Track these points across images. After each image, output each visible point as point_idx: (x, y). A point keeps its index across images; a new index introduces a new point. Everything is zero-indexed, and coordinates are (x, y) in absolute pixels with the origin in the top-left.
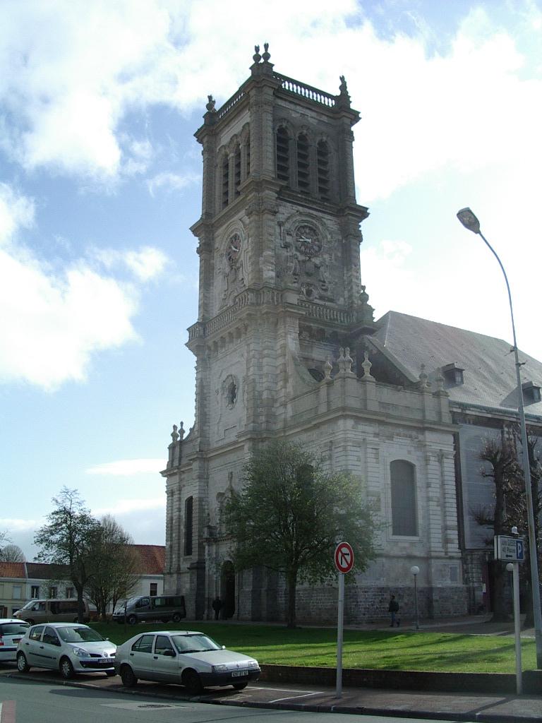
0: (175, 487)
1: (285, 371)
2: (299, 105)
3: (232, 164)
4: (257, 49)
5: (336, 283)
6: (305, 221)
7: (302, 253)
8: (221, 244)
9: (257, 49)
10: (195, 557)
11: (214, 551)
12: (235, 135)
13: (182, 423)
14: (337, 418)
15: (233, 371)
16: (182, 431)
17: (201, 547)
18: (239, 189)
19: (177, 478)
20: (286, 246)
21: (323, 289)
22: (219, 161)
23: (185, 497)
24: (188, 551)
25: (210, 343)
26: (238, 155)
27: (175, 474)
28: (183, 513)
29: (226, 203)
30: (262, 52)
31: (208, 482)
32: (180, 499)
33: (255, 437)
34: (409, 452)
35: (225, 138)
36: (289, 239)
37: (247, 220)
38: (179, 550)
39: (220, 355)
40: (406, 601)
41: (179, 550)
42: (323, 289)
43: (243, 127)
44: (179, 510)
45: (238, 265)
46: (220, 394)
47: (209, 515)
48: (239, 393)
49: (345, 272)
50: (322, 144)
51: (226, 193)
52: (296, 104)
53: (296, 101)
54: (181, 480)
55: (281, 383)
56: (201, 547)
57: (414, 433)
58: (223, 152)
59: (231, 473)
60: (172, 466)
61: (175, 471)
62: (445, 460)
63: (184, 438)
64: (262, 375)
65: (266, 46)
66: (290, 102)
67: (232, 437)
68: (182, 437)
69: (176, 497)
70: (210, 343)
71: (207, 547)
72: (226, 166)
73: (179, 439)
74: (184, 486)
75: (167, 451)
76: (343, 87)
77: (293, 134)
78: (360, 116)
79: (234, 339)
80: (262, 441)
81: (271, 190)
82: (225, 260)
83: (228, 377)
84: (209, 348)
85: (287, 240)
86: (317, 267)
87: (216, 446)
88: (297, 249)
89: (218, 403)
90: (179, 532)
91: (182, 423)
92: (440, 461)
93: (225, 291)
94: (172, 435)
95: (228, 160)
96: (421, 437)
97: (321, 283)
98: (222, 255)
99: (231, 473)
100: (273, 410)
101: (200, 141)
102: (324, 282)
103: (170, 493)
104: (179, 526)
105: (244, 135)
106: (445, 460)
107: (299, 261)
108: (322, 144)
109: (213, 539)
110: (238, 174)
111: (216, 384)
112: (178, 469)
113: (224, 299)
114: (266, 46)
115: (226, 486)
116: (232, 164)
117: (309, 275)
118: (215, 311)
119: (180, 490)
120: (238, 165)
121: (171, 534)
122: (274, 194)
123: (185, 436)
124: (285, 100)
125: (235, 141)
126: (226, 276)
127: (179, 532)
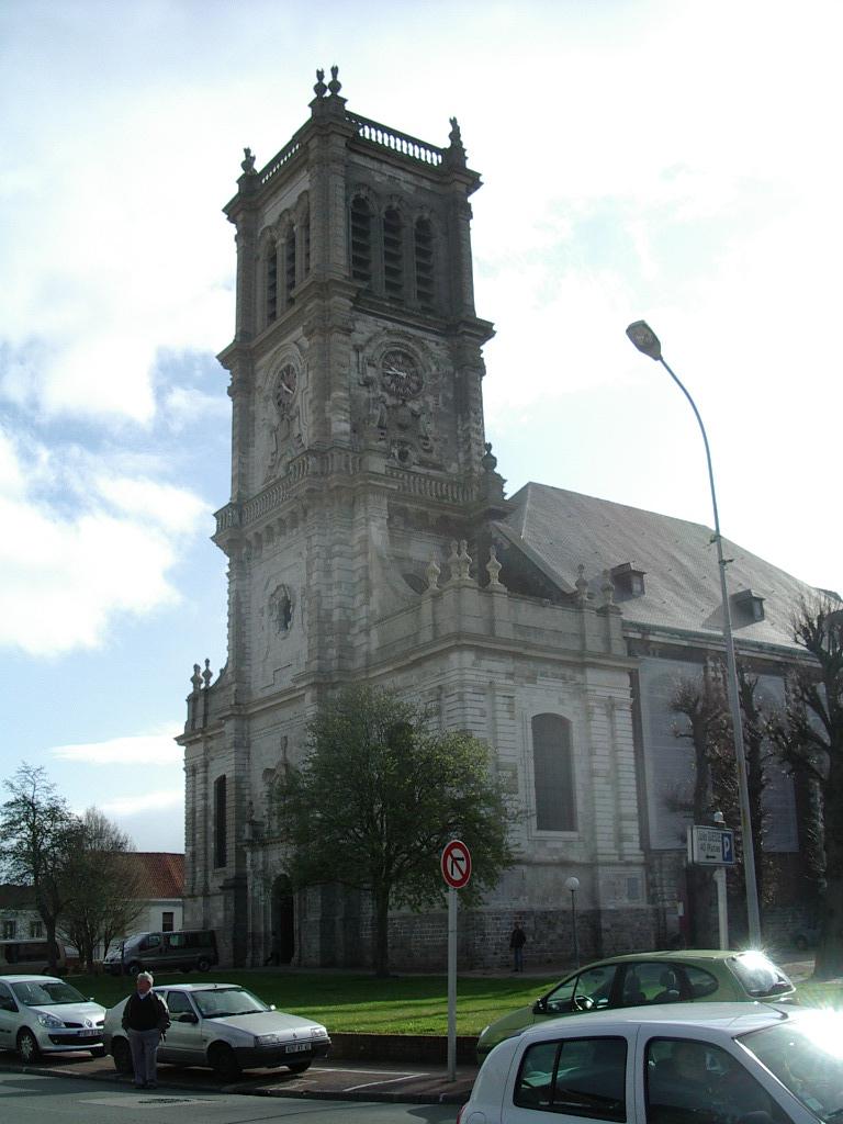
0: (199, 761)
1: (367, 578)
2: (386, 163)
3: (282, 254)
4: (320, 75)
5: (445, 441)
6: (398, 344)
7: (391, 393)
8: (265, 380)
9: (320, 75)
10: (230, 870)
11: (261, 860)
12: (286, 210)
13: (207, 662)
14: (450, 650)
15: (286, 579)
16: (208, 674)
17: (240, 855)
18: (293, 294)
19: (200, 748)
20: (368, 383)
21: (425, 450)
22: (262, 251)
23: (214, 776)
24: (221, 860)
25: (250, 536)
26: (292, 242)
27: (197, 741)
28: (211, 802)
29: (273, 316)
30: (327, 80)
31: (249, 753)
32: (206, 781)
33: (322, 680)
34: (561, 701)
35: (271, 216)
36: (371, 372)
37: (306, 343)
38: (206, 859)
39: (265, 555)
40: (560, 931)
41: (206, 859)
42: (425, 450)
43: (300, 197)
44: (205, 797)
45: (292, 413)
46: (266, 615)
47: (251, 803)
48: (296, 613)
49: (459, 422)
50: (422, 225)
51: (273, 302)
52: (381, 161)
53: (381, 157)
54: (207, 751)
55: (360, 597)
56: (240, 855)
57: (569, 672)
58: (268, 236)
59: (286, 737)
60: (193, 729)
61: (199, 736)
62: (617, 713)
63: (211, 685)
64: (331, 585)
65: (335, 71)
66: (373, 158)
67: (286, 682)
68: (207, 682)
69: (200, 776)
70: (250, 536)
71: (249, 854)
72: (273, 259)
73: (203, 686)
74: (212, 759)
75: (185, 706)
76: (455, 135)
77: (378, 209)
78: (481, 179)
79: (288, 530)
80: (333, 688)
81: (343, 296)
82: (272, 406)
83: (278, 588)
84: (249, 543)
85: (369, 374)
86: (415, 416)
87: (260, 695)
88: (384, 388)
89: (263, 625)
90: (206, 832)
91: (207, 662)
92: (610, 715)
93: (273, 454)
94: (192, 680)
95: (275, 250)
96: (579, 677)
97: (422, 441)
98: (266, 399)
99: (286, 737)
100: (349, 638)
101: (232, 219)
102: (427, 438)
103: (191, 771)
104: (206, 821)
105: (300, 209)
106: (617, 713)
107: (387, 407)
108: (422, 225)
109: (259, 841)
110: (292, 272)
111: (260, 600)
112: (203, 732)
113: (271, 467)
114: (335, 71)
115: (278, 758)
116: (282, 254)
117: (403, 427)
118: (257, 485)
119: (206, 765)
120: (292, 257)
121: (194, 835)
122: (348, 301)
123: (213, 681)
124: (365, 155)
125: (287, 219)
126: (274, 430)
127: (206, 832)
